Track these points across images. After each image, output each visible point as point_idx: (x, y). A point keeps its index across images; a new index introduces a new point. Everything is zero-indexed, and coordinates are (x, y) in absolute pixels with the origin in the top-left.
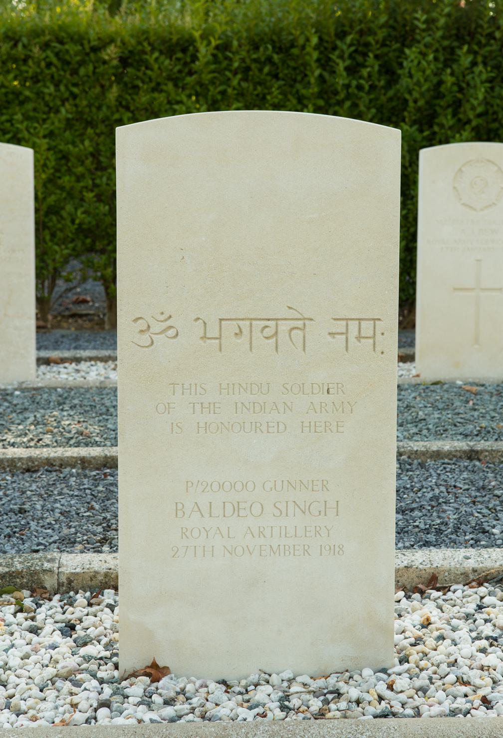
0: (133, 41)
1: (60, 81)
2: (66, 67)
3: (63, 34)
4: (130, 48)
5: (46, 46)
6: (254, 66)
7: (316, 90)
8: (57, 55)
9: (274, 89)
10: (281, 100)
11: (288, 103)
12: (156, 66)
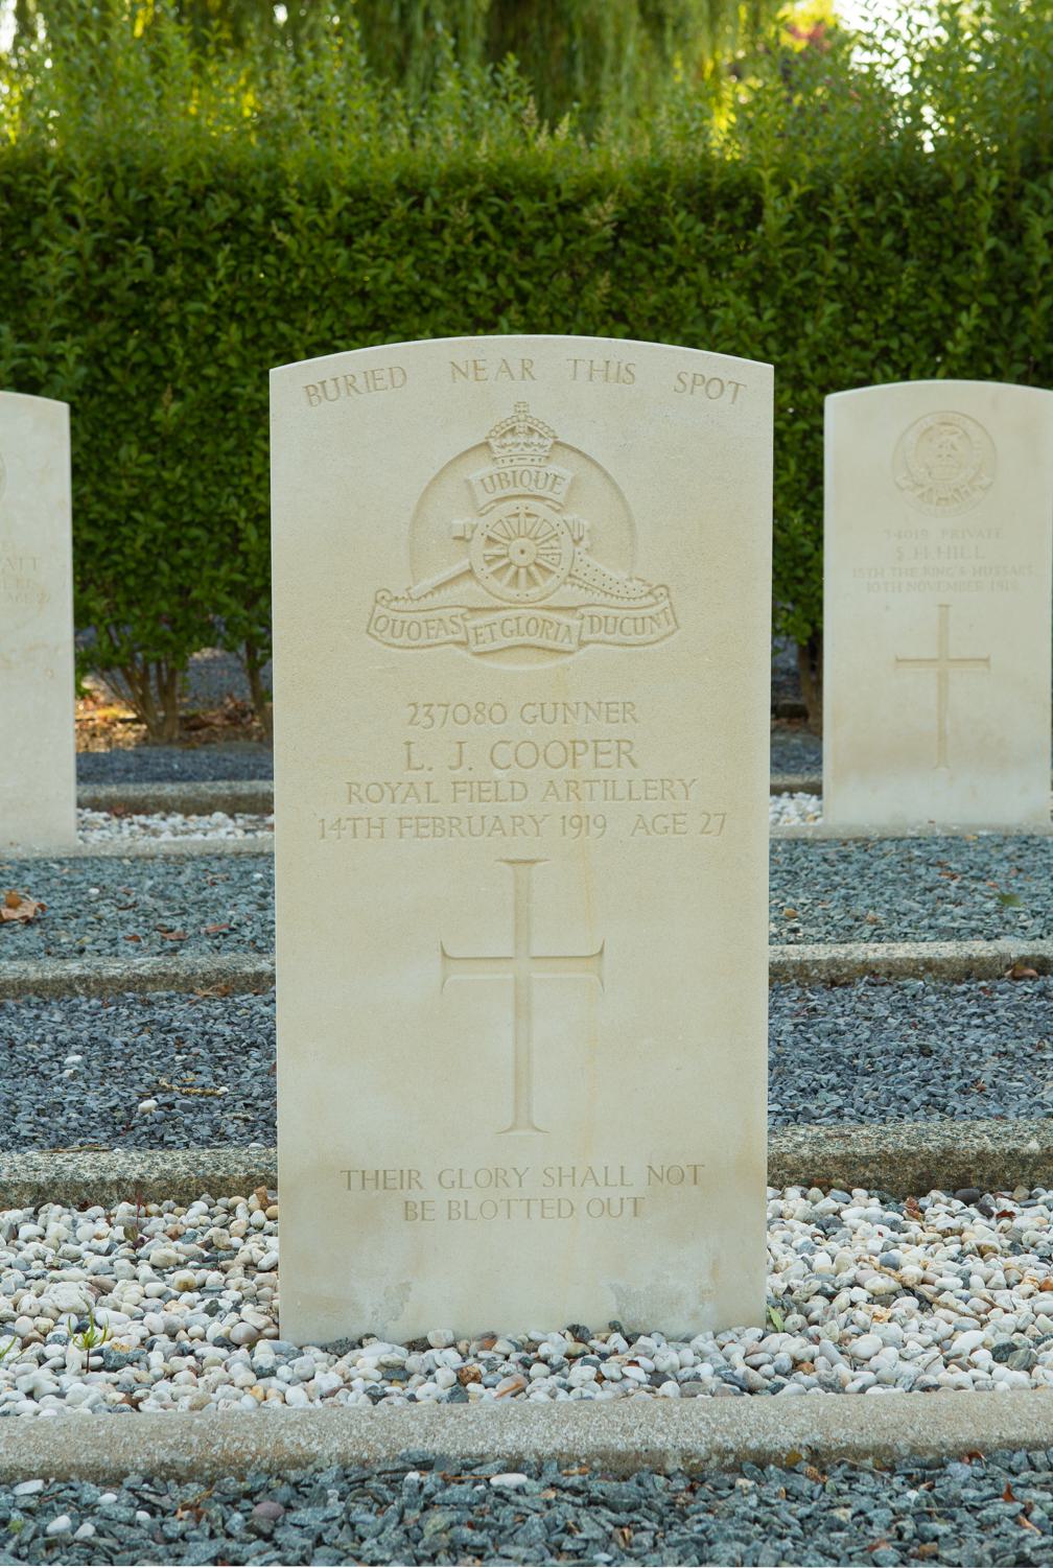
0: (638, 192)
1: (498, 268)
2: (511, 242)
3: (508, 180)
4: (631, 204)
5: (476, 201)
6: (862, 232)
7: (984, 275)
8: (496, 219)
9: (904, 276)
10: (910, 296)
11: (926, 302)
12: (680, 237)
